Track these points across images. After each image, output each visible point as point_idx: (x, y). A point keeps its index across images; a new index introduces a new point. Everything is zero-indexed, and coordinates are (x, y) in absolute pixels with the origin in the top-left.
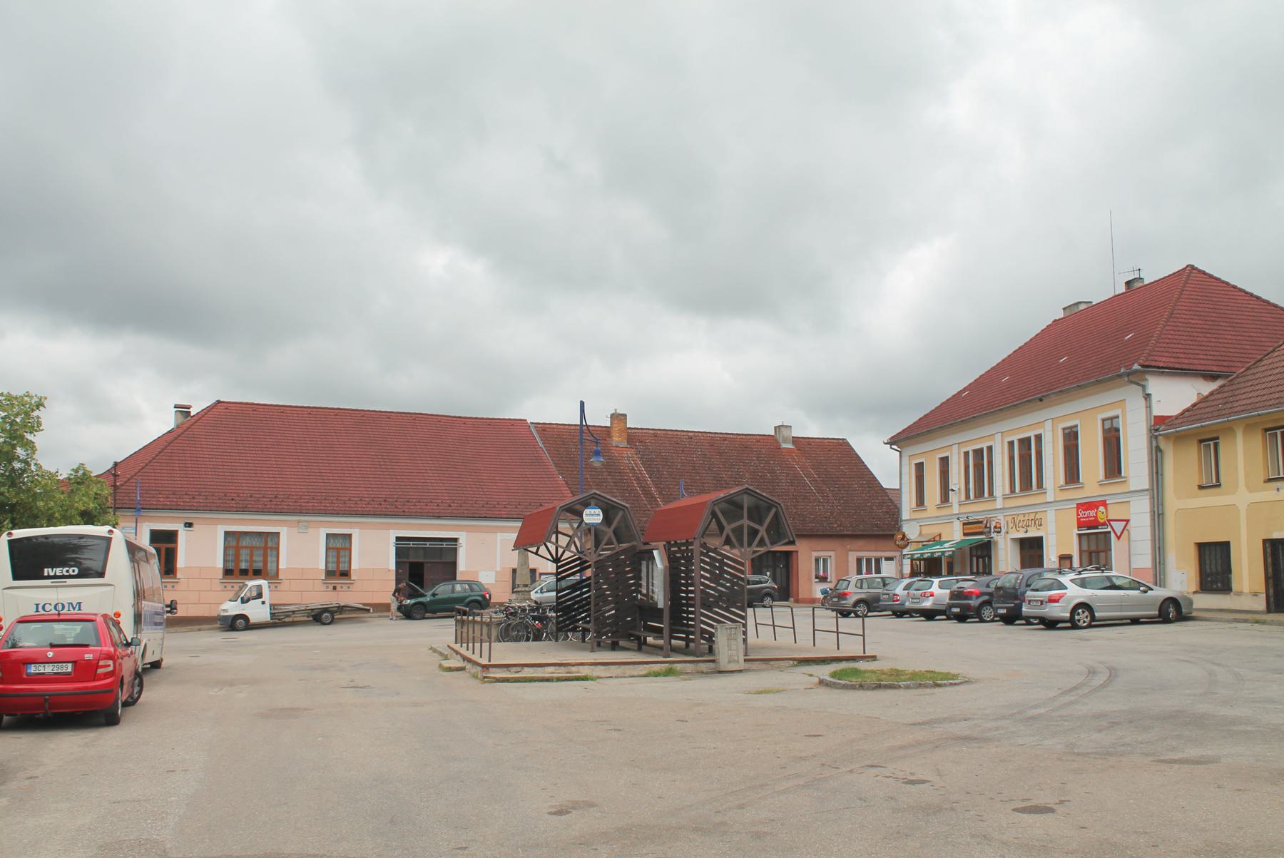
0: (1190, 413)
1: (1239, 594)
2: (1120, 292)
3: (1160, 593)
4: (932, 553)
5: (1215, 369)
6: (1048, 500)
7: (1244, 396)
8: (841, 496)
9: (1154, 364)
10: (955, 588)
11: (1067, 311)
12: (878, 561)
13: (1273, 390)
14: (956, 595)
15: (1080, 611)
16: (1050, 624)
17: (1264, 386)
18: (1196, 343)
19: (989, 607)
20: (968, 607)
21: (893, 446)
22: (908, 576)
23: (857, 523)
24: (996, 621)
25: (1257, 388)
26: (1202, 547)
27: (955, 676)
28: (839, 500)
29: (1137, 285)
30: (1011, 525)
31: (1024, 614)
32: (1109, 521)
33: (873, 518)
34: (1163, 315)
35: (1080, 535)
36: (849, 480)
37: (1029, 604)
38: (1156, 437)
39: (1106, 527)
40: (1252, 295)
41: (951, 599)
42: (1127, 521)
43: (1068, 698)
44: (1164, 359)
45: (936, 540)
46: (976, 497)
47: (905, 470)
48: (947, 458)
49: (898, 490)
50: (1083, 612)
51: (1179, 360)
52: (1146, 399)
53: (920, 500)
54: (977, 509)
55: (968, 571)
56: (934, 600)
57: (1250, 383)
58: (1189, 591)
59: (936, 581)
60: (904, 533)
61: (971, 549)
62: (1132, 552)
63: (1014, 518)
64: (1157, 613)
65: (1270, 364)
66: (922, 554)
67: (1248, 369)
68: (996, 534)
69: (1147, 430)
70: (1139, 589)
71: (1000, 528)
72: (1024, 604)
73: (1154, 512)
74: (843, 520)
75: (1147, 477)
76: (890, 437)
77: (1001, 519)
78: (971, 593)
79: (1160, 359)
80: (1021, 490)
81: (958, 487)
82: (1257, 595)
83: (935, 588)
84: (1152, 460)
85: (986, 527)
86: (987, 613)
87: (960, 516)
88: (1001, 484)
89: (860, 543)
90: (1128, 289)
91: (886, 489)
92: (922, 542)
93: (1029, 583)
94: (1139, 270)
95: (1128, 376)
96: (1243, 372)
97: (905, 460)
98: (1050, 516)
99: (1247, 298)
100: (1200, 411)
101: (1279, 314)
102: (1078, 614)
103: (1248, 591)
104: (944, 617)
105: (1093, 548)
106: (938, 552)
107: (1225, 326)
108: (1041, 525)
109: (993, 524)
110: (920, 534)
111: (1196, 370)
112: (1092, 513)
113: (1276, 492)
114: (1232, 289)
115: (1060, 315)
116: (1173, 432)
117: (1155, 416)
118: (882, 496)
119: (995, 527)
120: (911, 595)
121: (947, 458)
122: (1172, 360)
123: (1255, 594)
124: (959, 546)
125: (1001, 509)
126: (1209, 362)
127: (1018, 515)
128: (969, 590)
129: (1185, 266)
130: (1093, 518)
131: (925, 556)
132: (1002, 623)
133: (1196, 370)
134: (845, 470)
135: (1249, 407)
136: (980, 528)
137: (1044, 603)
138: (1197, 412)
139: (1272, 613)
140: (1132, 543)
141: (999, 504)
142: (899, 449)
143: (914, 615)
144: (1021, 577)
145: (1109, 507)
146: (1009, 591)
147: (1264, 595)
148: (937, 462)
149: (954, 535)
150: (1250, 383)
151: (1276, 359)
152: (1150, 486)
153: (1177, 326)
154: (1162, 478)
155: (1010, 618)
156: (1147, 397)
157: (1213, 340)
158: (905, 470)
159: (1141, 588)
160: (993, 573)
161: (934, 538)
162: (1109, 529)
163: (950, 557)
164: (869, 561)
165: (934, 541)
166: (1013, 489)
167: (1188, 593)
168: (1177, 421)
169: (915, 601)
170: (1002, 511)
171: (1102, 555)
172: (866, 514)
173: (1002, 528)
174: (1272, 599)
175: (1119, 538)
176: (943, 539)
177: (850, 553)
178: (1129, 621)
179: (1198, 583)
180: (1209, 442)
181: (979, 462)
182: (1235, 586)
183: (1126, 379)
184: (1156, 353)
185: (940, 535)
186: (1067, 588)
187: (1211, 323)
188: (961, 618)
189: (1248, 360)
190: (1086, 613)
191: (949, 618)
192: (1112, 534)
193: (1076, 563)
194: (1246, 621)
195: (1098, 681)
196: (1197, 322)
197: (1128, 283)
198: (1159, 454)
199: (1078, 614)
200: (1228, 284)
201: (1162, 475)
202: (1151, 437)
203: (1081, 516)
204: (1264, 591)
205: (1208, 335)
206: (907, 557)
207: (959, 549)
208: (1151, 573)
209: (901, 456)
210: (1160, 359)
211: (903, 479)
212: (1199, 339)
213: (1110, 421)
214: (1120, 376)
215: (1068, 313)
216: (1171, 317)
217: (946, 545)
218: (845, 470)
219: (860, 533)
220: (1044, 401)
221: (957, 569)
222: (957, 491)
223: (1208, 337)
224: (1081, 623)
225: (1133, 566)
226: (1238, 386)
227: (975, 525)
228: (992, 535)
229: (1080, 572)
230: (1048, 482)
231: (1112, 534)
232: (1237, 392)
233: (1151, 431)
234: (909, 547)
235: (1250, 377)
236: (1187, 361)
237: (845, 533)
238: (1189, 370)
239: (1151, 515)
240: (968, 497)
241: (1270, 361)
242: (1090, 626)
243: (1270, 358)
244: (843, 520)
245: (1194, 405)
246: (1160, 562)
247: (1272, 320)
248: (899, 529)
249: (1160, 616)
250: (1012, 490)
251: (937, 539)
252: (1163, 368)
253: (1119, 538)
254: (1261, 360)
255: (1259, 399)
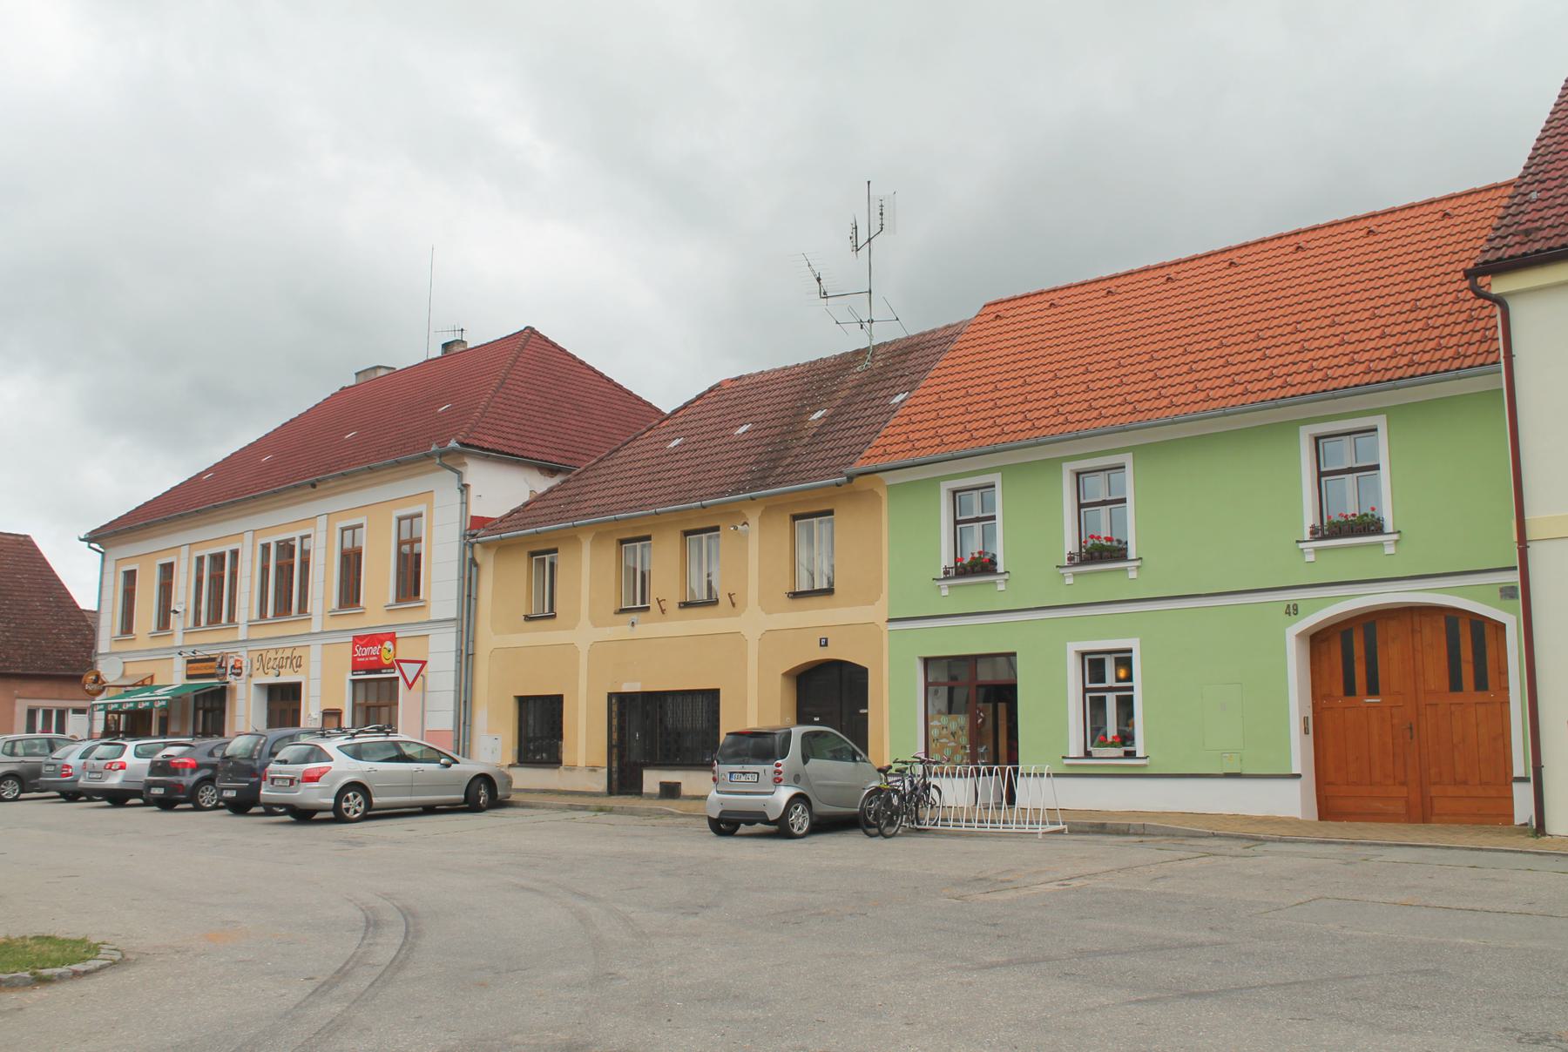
0: (518, 516)
1: (572, 768)
2: (435, 356)
3: (468, 768)
4: (136, 703)
5: (555, 461)
6: (313, 631)
7: (595, 495)
8: (12, 617)
9: (476, 443)
10: (159, 757)
11: (361, 375)
12: (62, 714)
13: (634, 488)
14: (160, 767)
15: (350, 794)
16: (303, 815)
17: (621, 483)
18: (533, 424)
19: (210, 787)
20: (179, 787)
21: (92, 545)
22: (99, 736)
23: (34, 657)
24: (222, 808)
25: (613, 485)
26: (523, 701)
27: (88, 949)
28: (9, 623)
29: (457, 349)
30: (256, 665)
31: (262, 800)
32: (398, 661)
33: (60, 651)
34: (482, 398)
35: (354, 682)
36: (27, 594)
37: (272, 783)
38: (472, 545)
39: (392, 670)
40: (602, 375)
41: (151, 773)
42: (424, 663)
43: (331, 1008)
44: (490, 439)
45: (146, 684)
46: (209, 623)
47: (109, 580)
48: (171, 565)
49: (95, 612)
50: (355, 797)
51: (510, 443)
52: (462, 491)
53: (127, 626)
54: (210, 641)
55: (190, 729)
56: (125, 775)
57: (603, 479)
58: (504, 764)
59: (131, 745)
60: (99, 672)
61: (196, 697)
62: (427, 708)
63: (261, 655)
64: (463, 796)
65: (630, 455)
66: (121, 704)
67: (601, 460)
68: (233, 676)
69: (460, 536)
70: (439, 762)
71: (241, 668)
72: (263, 783)
73: (462, 651)
74: (11, 652)
75: (455, 601)
76: (89, 531)
77: (243, 656)
78: (185, 764)
79: (486, 437)
80: (276, 615)
81: (183, 607)
82: (595, 771)
83: (129, 757)
84: (463, 578)
85: (220, 667)
86: (207, 796)
87: (183, 650)
88: (247, 606)
89: (35, 687)
90: (445, 353)
91: (84, 610)
92: (125, 686)
93: (274, 750)
94: (462, 330)
95: (440, 457)
96: (594, 464)
97: (110, 566)
98: (314, 655)
99: (596, 379)
100: (535, 513)
101: (633, 403)
102: (347, 800)
103: (584, 765)
104: (140, 801)
105: (372, 701)
106: (144, 701)
107: (569, 408)
108: (300, 666)
109: (231, 662)
110: (123, 675)
111: (532, 459)
112: (374, 650)
113: (629, 627)
114: (579, 365)
115: (352, 381)
116: (497, 539)
117: (472, 517)
118: (76, 621)
119: (233, 667)
120: (89, 767)
121: (171, 565)
122: (501, 441)
123: (593, 769)
124: (178, 693)
125: (244, 641)
126: (547, 450)
127: (268, 650)
128: (181, 760)
129: (523, 328)
130: (375, 658)
131: (125, 707)
132: (227, 812)
133: (532, 459)
134: (23, 580)
135: (602, 509)
136: (211, 667)
137: (296, 782)
138: (531, 513)
139: (614, 795)
140: (427, 694)
141: (242, 634)
142: (102, 550)
143: (95, 798)
144: (262, 741)
145: (399, 642)
146: (243, 762)
147: (606, 770)
148: (157, 571)
149: (174, 676)
150: (603, 479)
151: (639, 450)
152: (458, 615)
153: (509, 399)
154: (476, 603)
155: (242, 805)
156: (464, 488)
157: (554, 423)
158: (109, 580)
159: (442, 761)
160: (226, 735)
161: (143, 681)
162: (397, 674)
163: (163, 709)
164: (47, 713)
165: (143, 685)
166: (264, 612)
167: (502, 766)
168: (503, 525)
169: (95, 776)
170: (244, 644)
171: (384, 711)
172: (50, 645)
173: (244, 669)
174: (615, 776)
175: (410, 686)
176: (155, 684)
177: (18, 701)
178: (421, 809)
179: (516, 753)
180: (542, 556)
181: (219, 571)
182: (566, 757)
183: (438, 461)
184: (480, 430)
185: (152, 677)
186: (331, 760)
187: (552, 402)
188: (166, 804)
189: (603, 449)
190: (360, 798)
191: (147, 804)
192: (401, 680)
193: (346, 721)
194: (585, 808)
195: (386, 947)
196: (534, 397)
197: (446, 346)
198: (474, 569)
199: (347, 800)
200: (574, 357)
201: (476, 599)
202: (465, 545)
203: (358, 654)
204: (606, 765)
205: (548, 416)
206: (99, 707)
207: (178, 699)
208: (452, 737)
209: (103, 560)
210: (486, 437)
211: (104, 593)
212: (536, 419)
213: (409, 521)
214: (429, 457)
215: (362, 380)
216: (501, 387)
217: (160, 692)
218: (23, 580)
219: (37, 672)
220: (318, 487)
221: (173, 727)
222: (182, 614)
223: (548, 419)
224: (350, 814)
225: (427, 728)
226: (587, 482)
227: (205, 664)
228: (228, 678)
229: (353, 735)
230: (315, 604)
231: (401, 680)
232: (586, 489)
233: (465, 536)
234: (105, 693)
235: (603, 471)
236: (519, 445)
237: (12, 671)
238: (522, 457)
239: (457, 656)
240: (197, 622)
241: (630, 452)
242: (365, 818)
243: (630, 448)
244: (11, 652)
245: (526, 505)
246: (465, 723)
247: (625, 409)
248: (91, 665)
249: (466, 800)
250: (263, 614)
251: (148, 682)
252: (488, 450)
253: (410, 686)
254: (618, 450)
255: (615, 499)
